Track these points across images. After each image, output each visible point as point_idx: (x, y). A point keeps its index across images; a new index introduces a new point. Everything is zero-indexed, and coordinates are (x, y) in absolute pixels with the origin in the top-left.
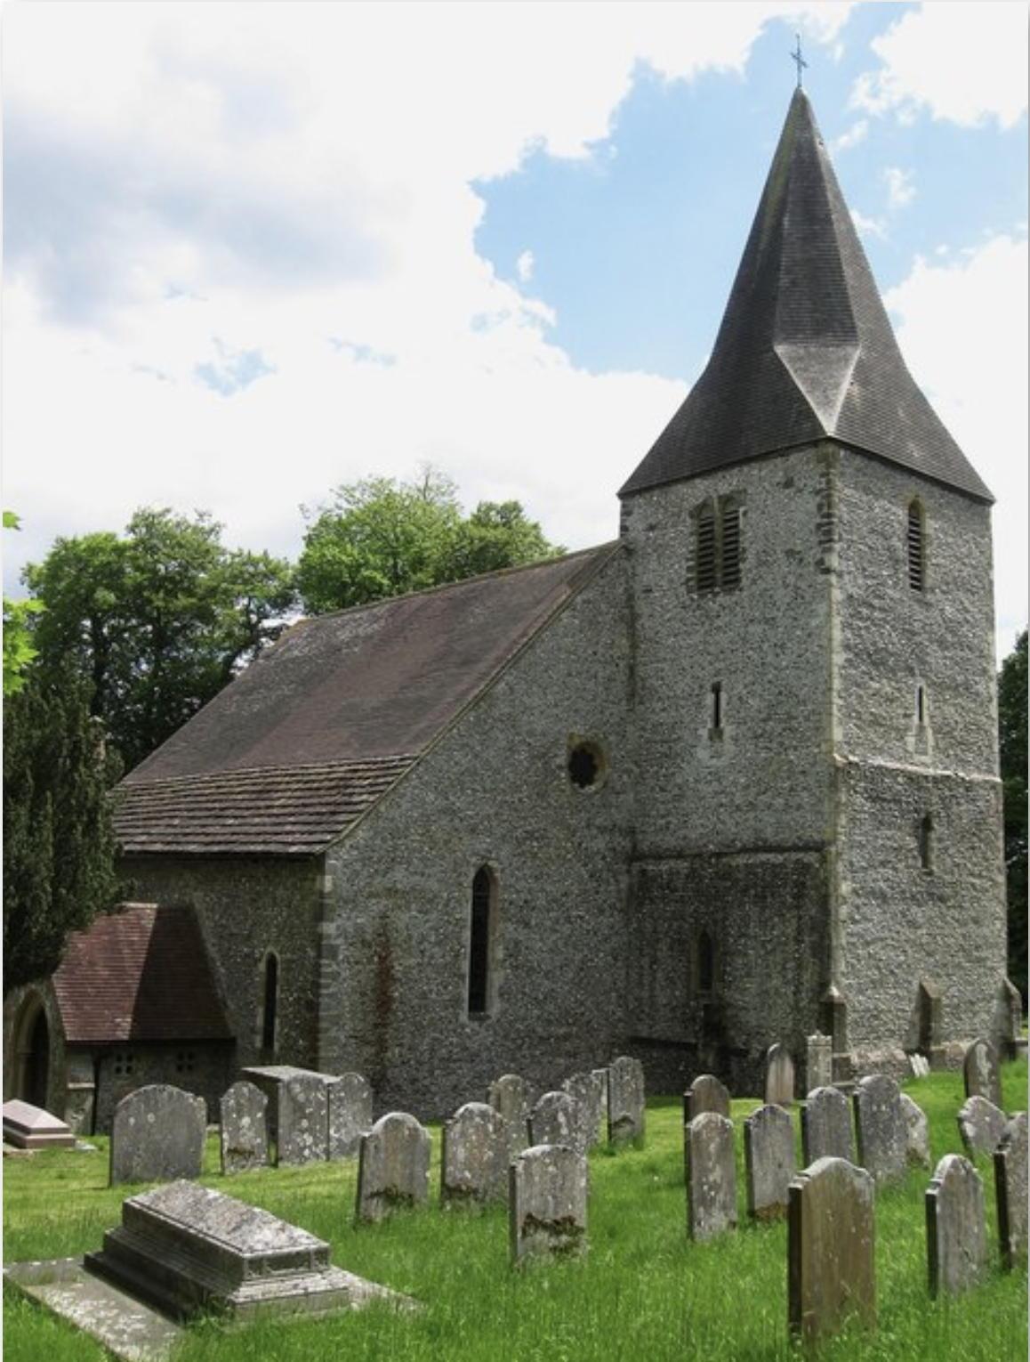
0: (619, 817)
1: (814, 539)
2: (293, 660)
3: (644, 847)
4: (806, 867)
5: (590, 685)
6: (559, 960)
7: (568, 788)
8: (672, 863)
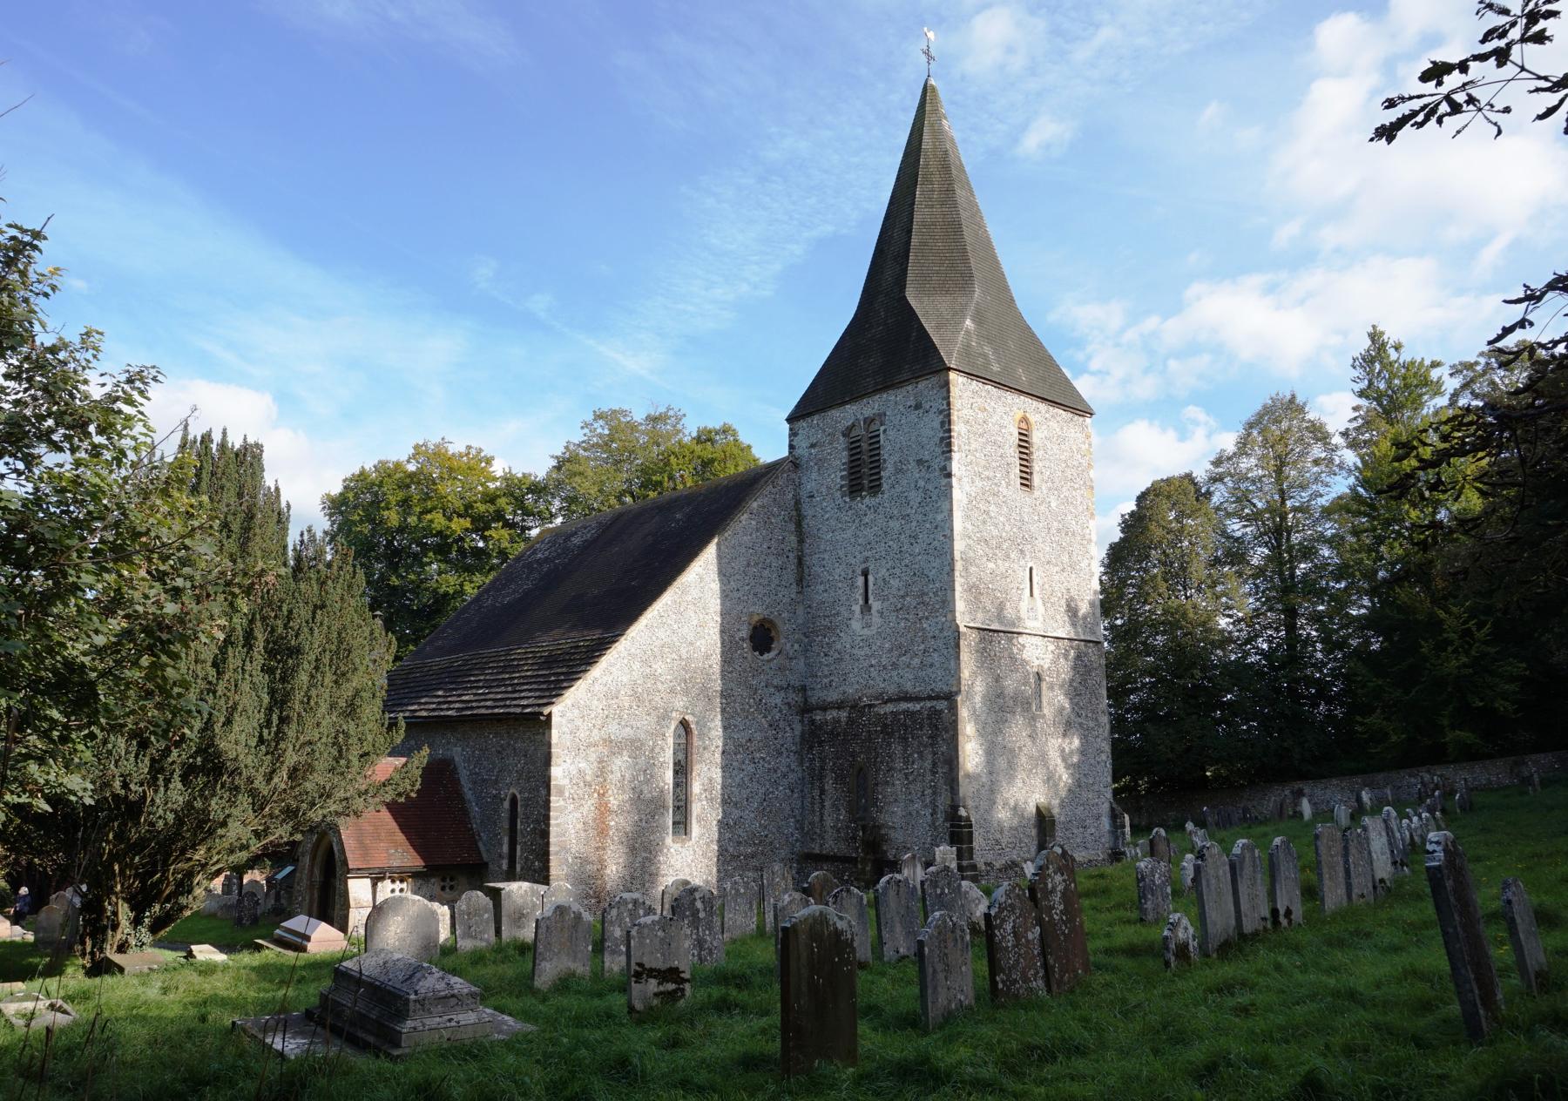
0: (795, 680)
1: (938, 450)
2: (537, 561)
3: (813, 701)
4: (935, 713)
5: (766, 573)
6: (745, 793)
7: (749, 656)
8: (835, 713)
